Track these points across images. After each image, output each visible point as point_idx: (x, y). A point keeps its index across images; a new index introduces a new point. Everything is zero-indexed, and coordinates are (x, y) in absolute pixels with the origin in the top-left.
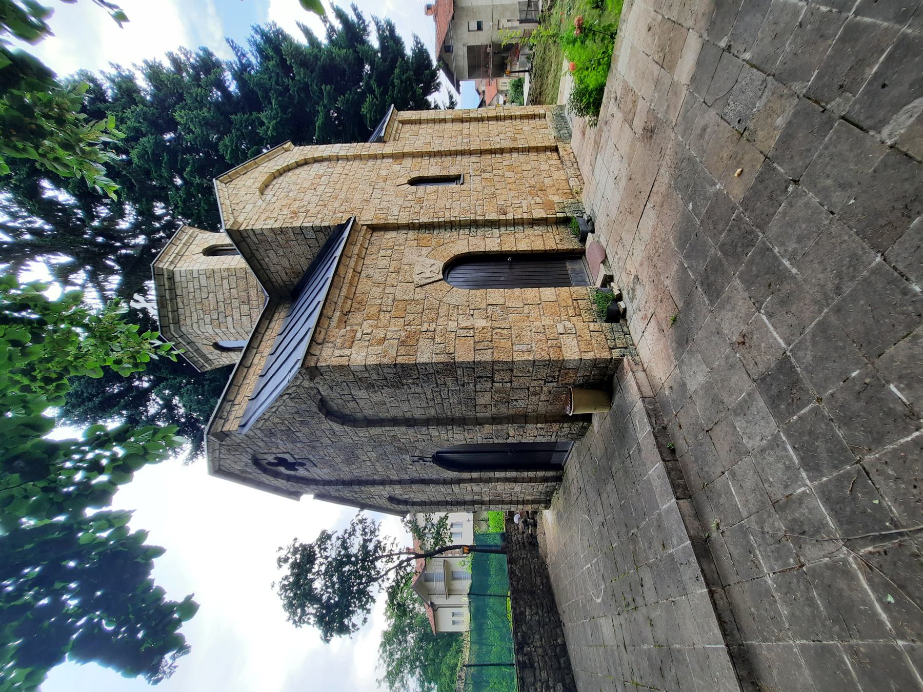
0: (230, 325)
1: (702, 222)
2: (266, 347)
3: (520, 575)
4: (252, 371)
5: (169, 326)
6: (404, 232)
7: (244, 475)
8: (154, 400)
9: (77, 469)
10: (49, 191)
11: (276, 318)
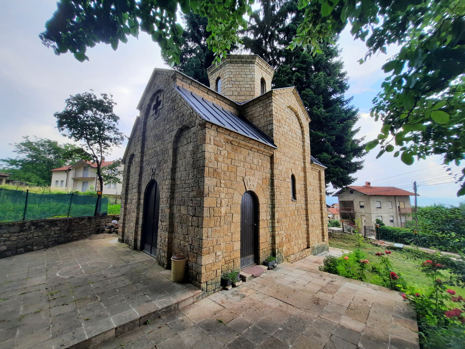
0: (228, 86)
1: (272, 337)
2: (217, 102)
3: (80, 223)
4: (206, 94)
6: (270, 171)
7: (153, 84)
8: (195, 45)
9: (162, 18)
10: (291, 16)
11: (231, 107)
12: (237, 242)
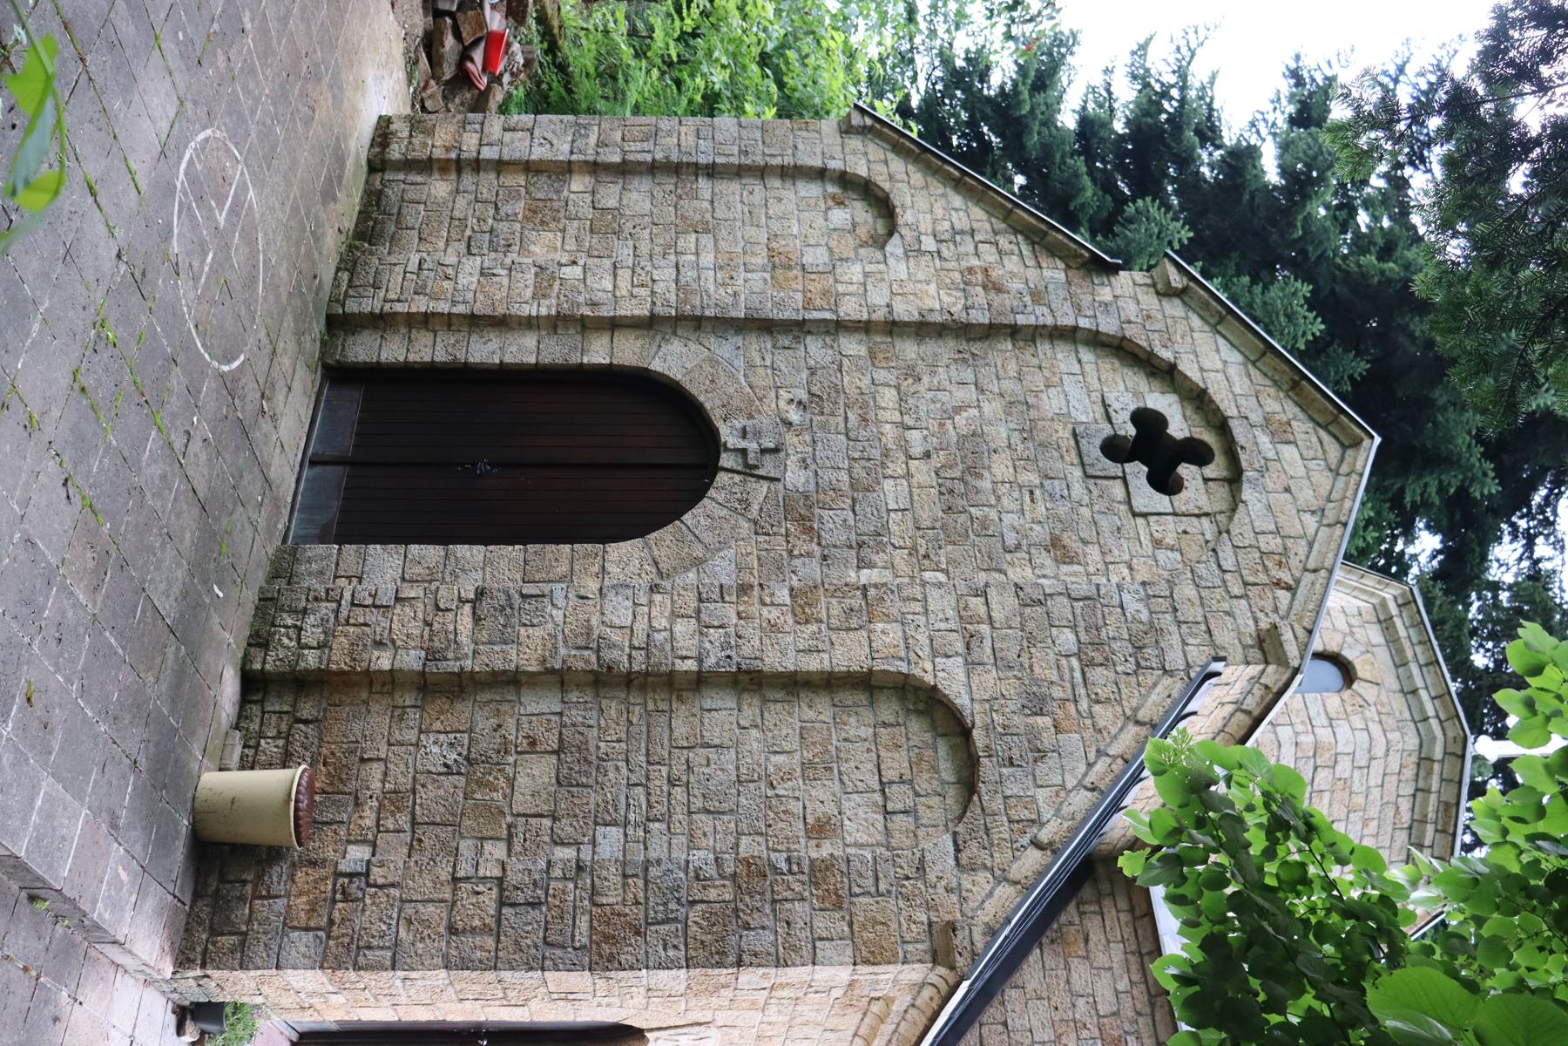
5: (1445, 753)
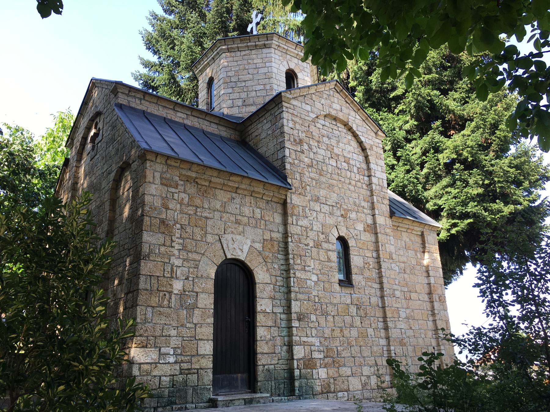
4: (171, 112)
12: (206, 342)
